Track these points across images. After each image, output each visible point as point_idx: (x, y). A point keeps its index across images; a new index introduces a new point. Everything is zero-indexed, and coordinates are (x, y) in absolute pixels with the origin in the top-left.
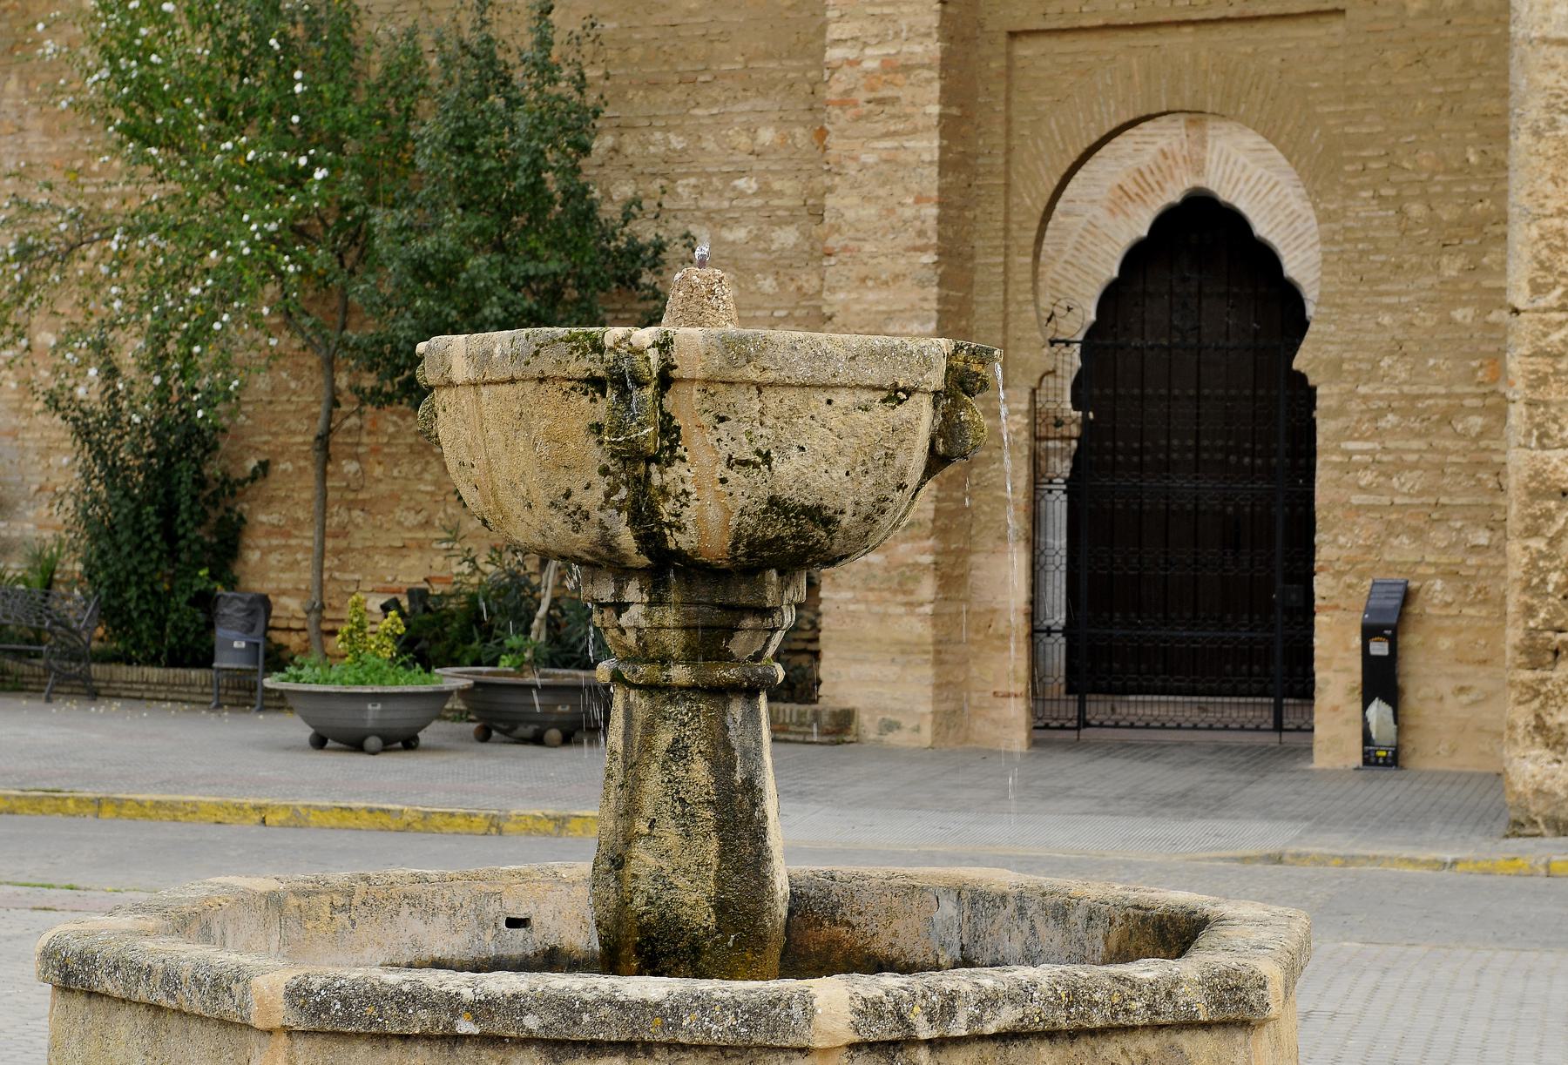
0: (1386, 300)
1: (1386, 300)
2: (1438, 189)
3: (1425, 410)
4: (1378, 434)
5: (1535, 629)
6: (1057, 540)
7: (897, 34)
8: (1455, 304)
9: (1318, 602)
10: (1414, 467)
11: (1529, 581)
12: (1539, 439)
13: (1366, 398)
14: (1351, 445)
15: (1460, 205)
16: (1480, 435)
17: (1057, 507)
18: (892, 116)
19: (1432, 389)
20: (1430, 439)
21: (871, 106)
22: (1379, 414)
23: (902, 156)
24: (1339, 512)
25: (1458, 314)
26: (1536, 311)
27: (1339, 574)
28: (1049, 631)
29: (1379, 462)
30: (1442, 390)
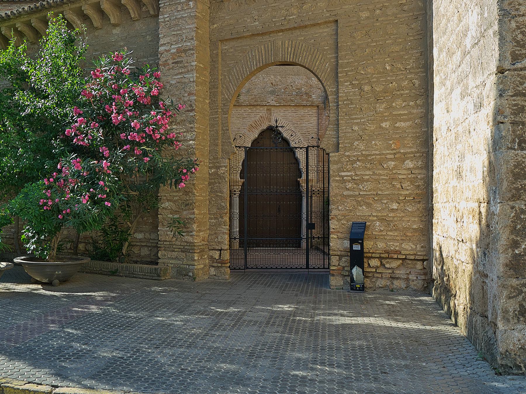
0: (355, 121)
1: (355, 121)
2: (374, 80)
3: (371, 160)
4: (354, 169)
5: (520, 255)
6: (236, 210)
7: (182, 40)
8: (382, 121)
9: (331, 230)
10: (367, 181)
11: (515, 228)
12: (519, 144)
13: (349, 156)
14: (343, 174)
15: (383, 85)
16: (394, 168)
17: (236, 200)
18: (181, 67)
19: (374, 152)
20: (373, 170)
21: (173, 65)
22: (355, 162)
23: (184, 80)
24: (339, 198)
25: (384, 125)
26: (515, 70)
27: (339, 220)
28: (235, 239)
29: (355, 180)
30: (377, 152)
